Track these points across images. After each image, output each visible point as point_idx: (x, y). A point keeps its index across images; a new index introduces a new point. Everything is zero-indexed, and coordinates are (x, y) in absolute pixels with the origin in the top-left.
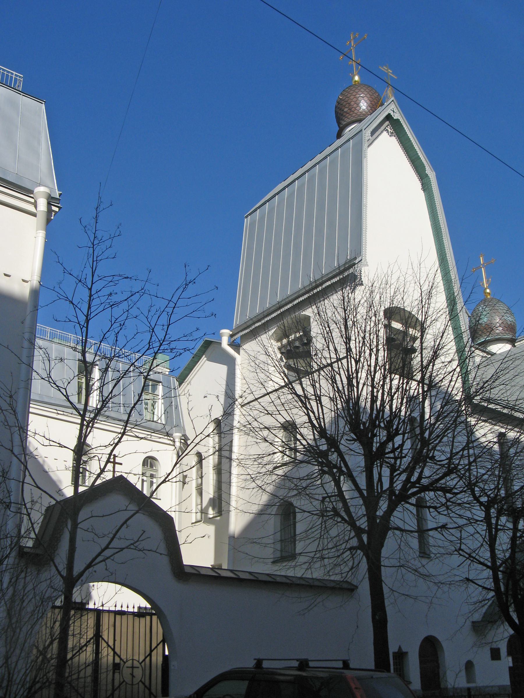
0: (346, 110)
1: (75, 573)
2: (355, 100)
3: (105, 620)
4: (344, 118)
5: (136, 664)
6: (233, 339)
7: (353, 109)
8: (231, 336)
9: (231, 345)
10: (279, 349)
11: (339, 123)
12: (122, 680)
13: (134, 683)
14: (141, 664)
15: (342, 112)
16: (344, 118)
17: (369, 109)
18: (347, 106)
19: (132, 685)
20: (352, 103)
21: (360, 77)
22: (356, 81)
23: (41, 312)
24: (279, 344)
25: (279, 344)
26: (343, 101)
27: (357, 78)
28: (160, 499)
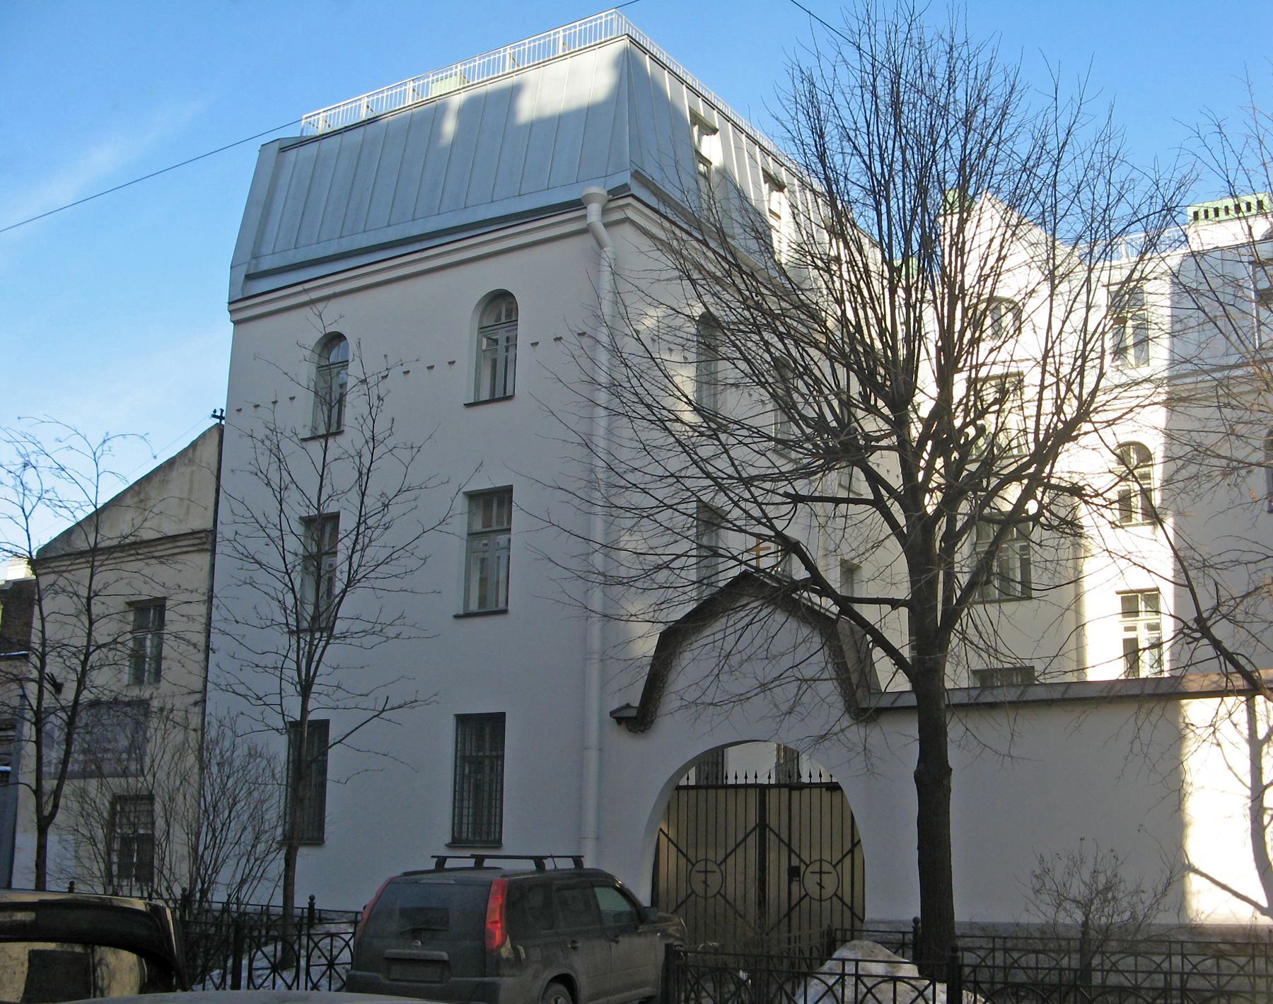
1: (46, 813)
5: (711, 866)
12: (803, 893)
13: (824, 897)
14: (834, 867)
19: (821, 900)
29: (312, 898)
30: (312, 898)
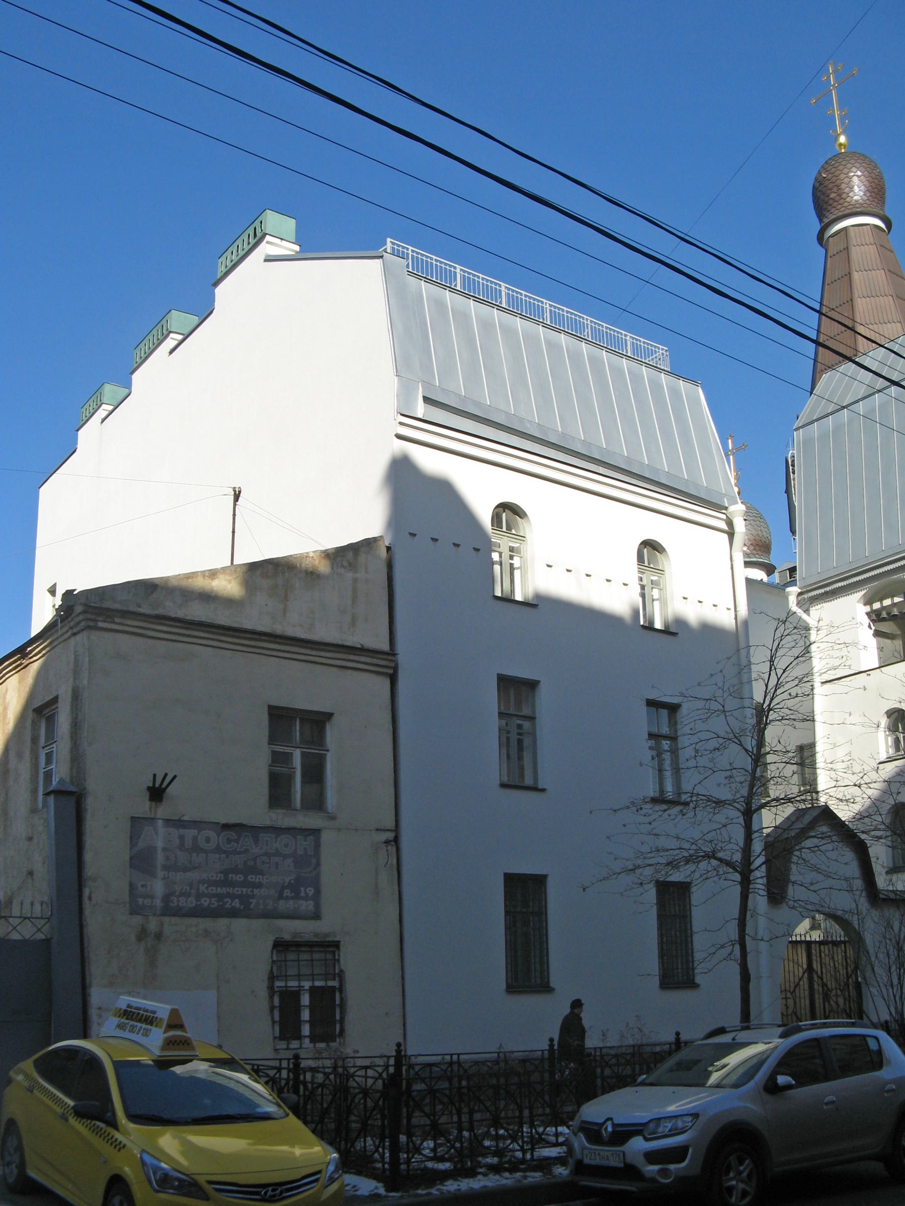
0: (832, 196)
2: (846, 180)
3: (815, 950)
4: (829, 208)
6: (800, 598)
7: (844, 196)
8: (800, 594)
9: (799, 604)
10: (868, 614)
11: (821, 221)
15: (826, 199)
16: (829, 208)
17: (868, 194)
18: (835, 190)
20: (843, 186)
21: (848, 137)
22: (841, 145)
23: (888, 641)
24: (868, 608)
25: (868, 608)
26: (827, 182)
27: (842, 139)
28: (543, 790)
29: (678, 1034)
30: (678, 1034)
